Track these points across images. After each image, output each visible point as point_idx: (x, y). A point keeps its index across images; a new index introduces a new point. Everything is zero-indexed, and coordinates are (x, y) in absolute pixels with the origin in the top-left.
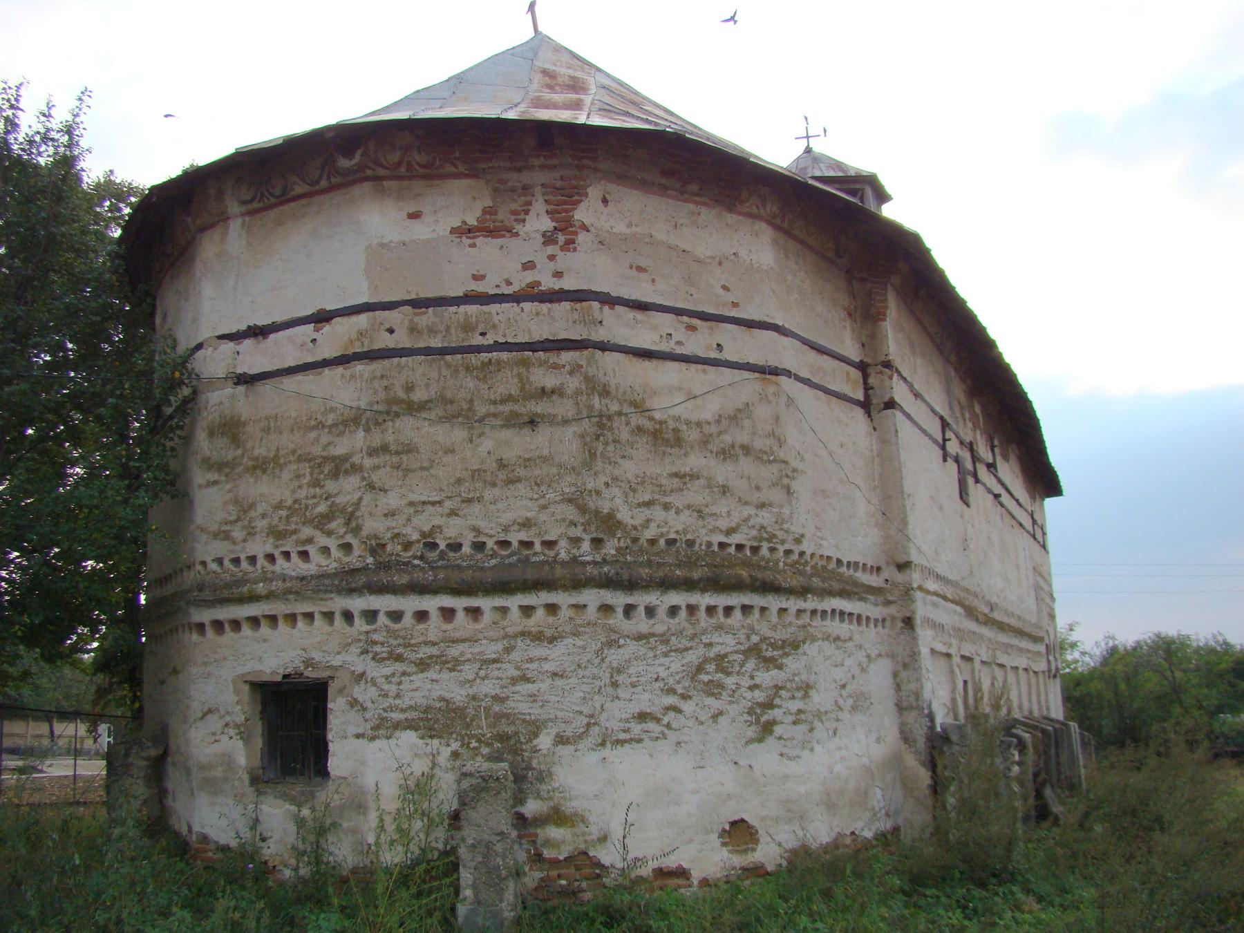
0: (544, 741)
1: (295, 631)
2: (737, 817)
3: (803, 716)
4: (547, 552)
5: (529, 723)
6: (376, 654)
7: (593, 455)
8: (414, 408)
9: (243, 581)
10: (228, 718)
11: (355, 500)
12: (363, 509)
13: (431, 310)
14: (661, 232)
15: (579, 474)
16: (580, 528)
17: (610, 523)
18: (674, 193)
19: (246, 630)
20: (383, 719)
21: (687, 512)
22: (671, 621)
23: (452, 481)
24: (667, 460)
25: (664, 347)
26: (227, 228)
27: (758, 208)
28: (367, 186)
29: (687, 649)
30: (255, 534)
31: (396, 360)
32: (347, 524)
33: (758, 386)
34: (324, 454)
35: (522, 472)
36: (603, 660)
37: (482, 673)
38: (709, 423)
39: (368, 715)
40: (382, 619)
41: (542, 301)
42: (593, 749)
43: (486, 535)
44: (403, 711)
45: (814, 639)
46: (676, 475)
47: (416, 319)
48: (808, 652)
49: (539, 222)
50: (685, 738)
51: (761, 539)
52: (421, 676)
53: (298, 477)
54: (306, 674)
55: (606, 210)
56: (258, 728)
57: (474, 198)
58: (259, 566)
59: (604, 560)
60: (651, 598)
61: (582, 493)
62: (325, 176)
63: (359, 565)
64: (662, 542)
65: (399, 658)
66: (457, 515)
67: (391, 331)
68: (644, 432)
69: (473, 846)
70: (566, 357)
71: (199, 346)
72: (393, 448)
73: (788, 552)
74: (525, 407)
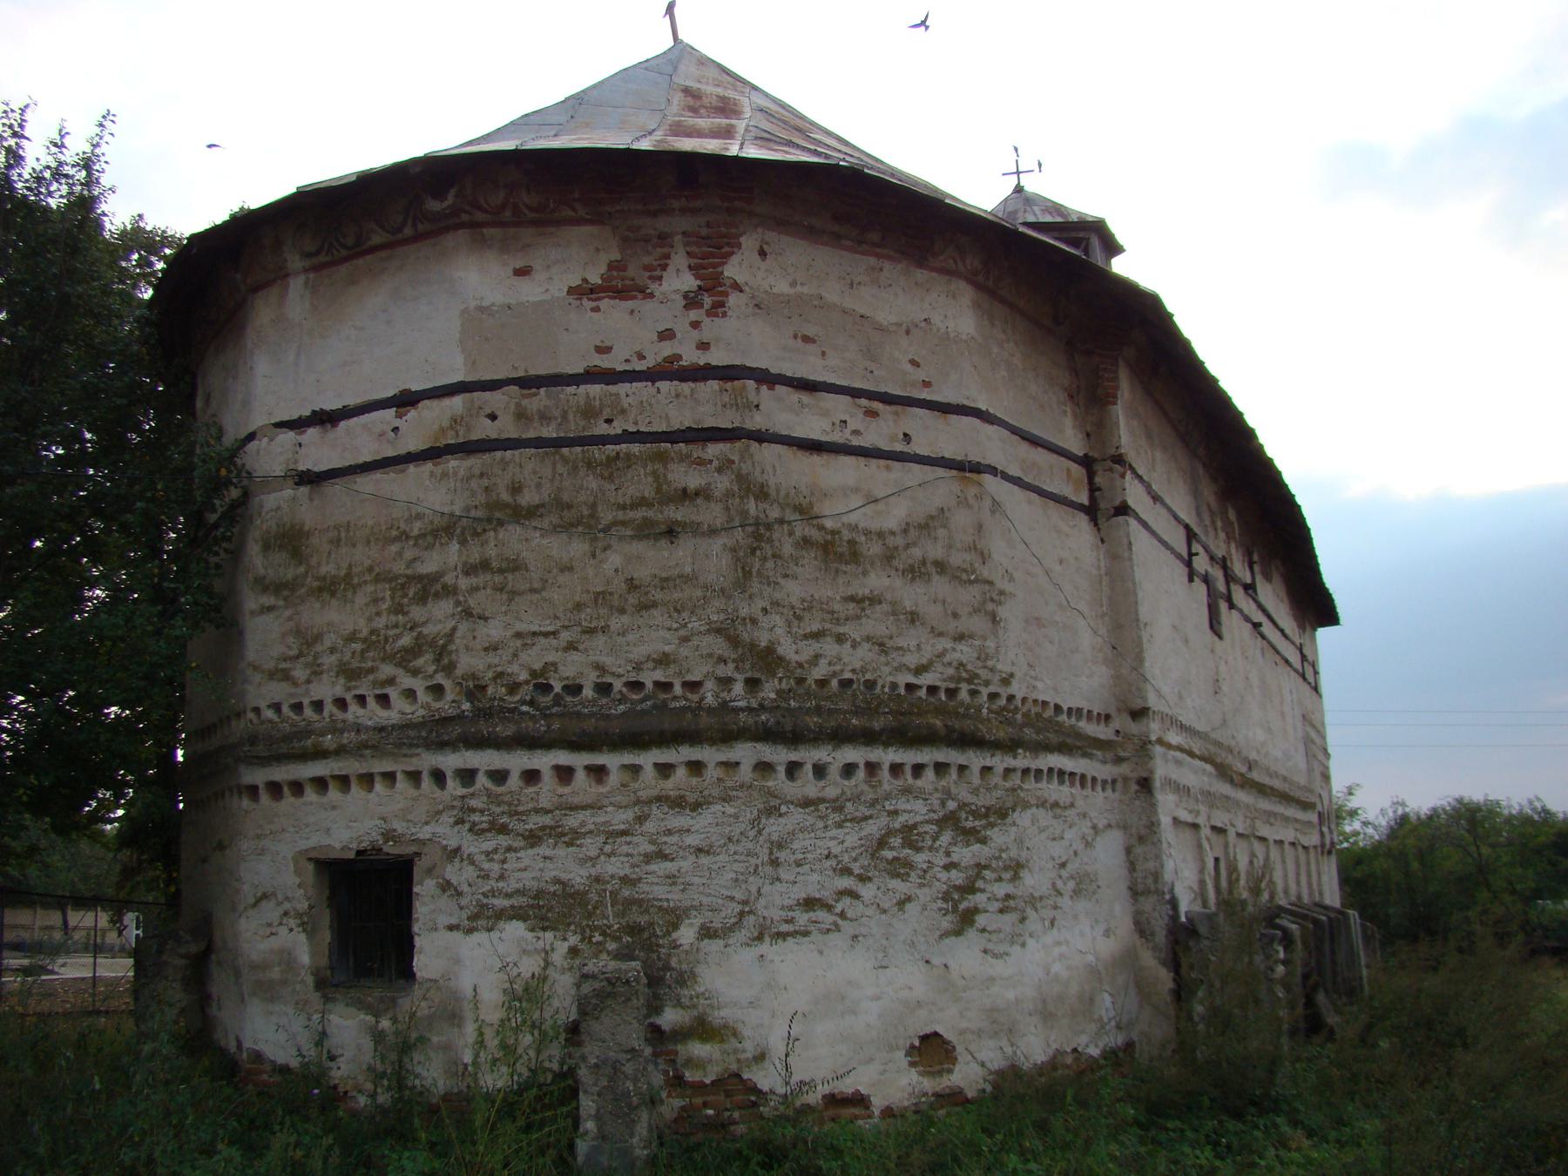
0: (686, 934)
1: (371, 796)
2: (928, 1030)
3: (1012, 903)
4: (689, 695)
5: (667, 911)
6: (474, 824)
7: (747, 574)
8: (522, 515)
9: (307, 733)
10: (287, 906)
11: (447, 630)
12: (457, 641)
13: (543, 390)
14: (833, 293)
15: (729, 597)
16: (731, 666)
17: (768, 659)
18: (849, 243)
19: (310, 795)
20: (483, 906)
21: (866, 646)
22: (846, 783)
23: (570, 606)
24: (840, 581)
25: (837, 437)
26: (286, 288)
27: (956, 262)
28: (463, 235)
29: (866, 818)
30: (322, 673)
31: (499, 454)
32: (438, 660)
33: (956, 487)
34: (409, 572)
35: (658, 595)
36: (760, 832)
37: (608, 848)
38: (893, 533)
39: (464, 902)
40: (482, 781)
41: (683, 380)
42: (748, 945)
43: (613, 674)
44: (508, 896)
45: (1026, 805)
46: (852, 599)
47: (525, 402)
48: (1018, 822)
49: (679, 280)
50: (863, 930)
51: (959, 680)
52: (530, 852)
53: (376, 601)
54: (386, 849)
55: (763, 265)
56: (326, 918)
57: (597, 250)
58: (326, 713)
59: (762, 706)
60: (821, 754)
61: (733, 621)
62: (410, 222)
63: (452, 712)
64: (834, 683)
65: (503, 830)
66: (576, 649)
67: (493, 417)
68: (812, 545)
69: (596, 1066)
70: (713, 450)
71: (251, 437)
72: (494, 564)
73: (993, 696)
74: (662, 512)
